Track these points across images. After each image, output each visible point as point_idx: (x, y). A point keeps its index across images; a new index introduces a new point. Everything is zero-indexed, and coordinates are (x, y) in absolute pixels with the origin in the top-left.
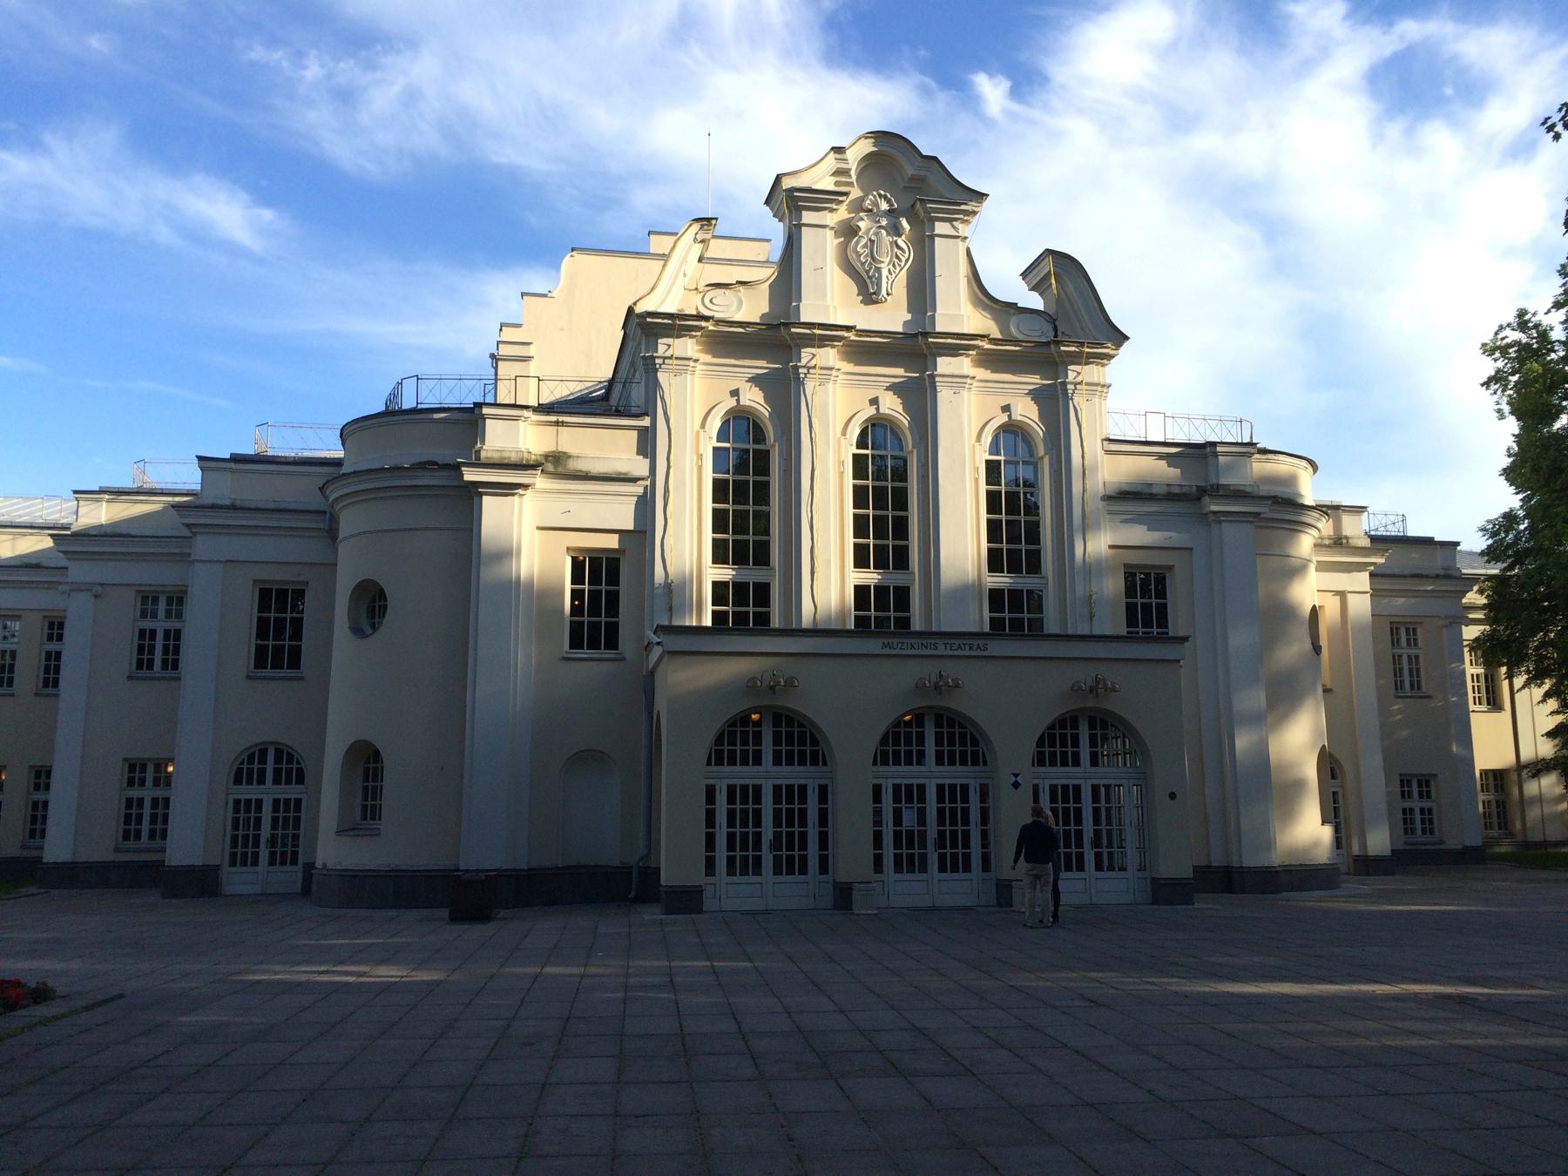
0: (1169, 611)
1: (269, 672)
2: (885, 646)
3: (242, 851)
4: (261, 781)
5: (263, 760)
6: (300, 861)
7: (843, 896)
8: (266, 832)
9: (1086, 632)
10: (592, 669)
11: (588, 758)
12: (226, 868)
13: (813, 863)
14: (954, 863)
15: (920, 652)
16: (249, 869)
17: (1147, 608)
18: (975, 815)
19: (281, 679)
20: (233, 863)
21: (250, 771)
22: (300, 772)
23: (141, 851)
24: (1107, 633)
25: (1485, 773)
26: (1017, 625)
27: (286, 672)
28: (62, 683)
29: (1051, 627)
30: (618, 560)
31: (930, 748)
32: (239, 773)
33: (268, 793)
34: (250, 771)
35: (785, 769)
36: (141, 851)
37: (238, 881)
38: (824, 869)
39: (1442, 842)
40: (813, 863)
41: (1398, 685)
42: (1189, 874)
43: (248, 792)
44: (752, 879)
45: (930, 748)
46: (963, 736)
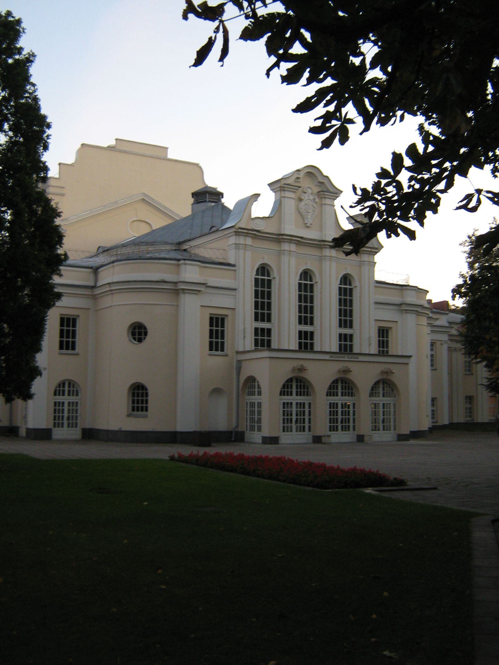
0: (338, 304)
2: (331, 357)
3: (58, 421)
5: (64, 386)
6: (79, 425)
7: (360, 439)
10: (217, 361)
11: (217, 391)
13: (351, 428)
14: (345, 428)
15: (342, 359)
19: (68, 354)
20: (55, 427)
22: (77, 392)
24: (194, 282)
25: (198, 6)
31: (294, 390)
32: (55, 391)
33: (66, 399)
35: (299, 397)
37: (58, 433)
38: (354, 430)
40: (351, 428)
41: (294, 192)
43: (59, 399)
45: (294, 390)
46: (304, 386)
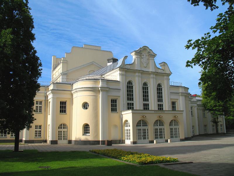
1: (62, 113)
4: (62, 128)
8: (63, 135)
9: (139, 109)
12: (58, 141)
16: (61, 140)
17: (114, 103)
18: (163, 132)
21: (60, 127)
23: (3, 138)
26: (146, 109)
27: (64, 113)
28: (169, 123)
29: (150, 109)
30: (116, 100)
31: (142, 124)
34: (60, 127)
35: (145, 128)
36: (3, 138)
39: (194, 134)
42: (184, 138)
44: (141, 140)
45: (142, 124)
46: (145, 123)
